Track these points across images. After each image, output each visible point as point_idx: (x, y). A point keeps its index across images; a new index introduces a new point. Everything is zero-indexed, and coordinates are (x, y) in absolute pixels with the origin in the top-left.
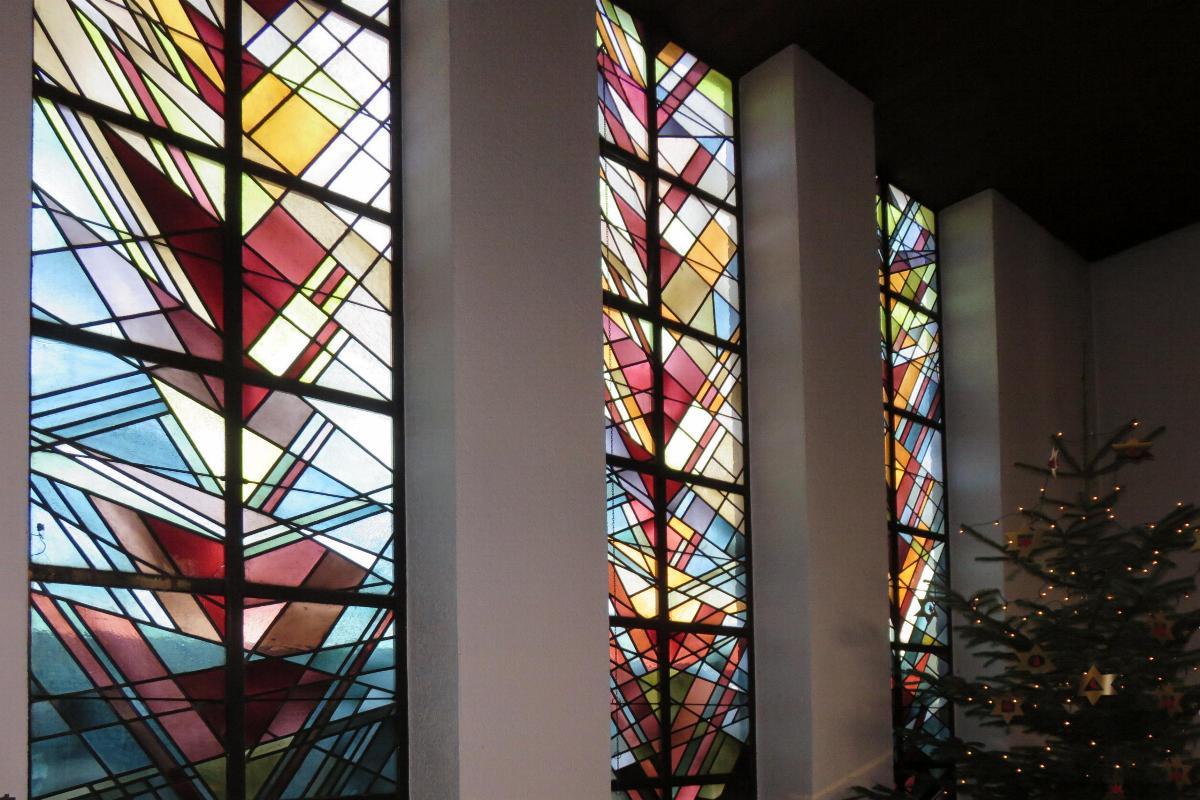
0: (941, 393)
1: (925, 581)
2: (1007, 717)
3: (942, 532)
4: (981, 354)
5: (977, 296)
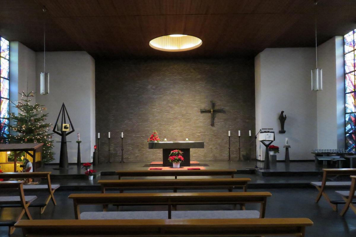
0: (9, 73)
1: (170, 217)
2: (15, 131)
3: (9, 98)
4: (15, 69)
5: (15, 58)
